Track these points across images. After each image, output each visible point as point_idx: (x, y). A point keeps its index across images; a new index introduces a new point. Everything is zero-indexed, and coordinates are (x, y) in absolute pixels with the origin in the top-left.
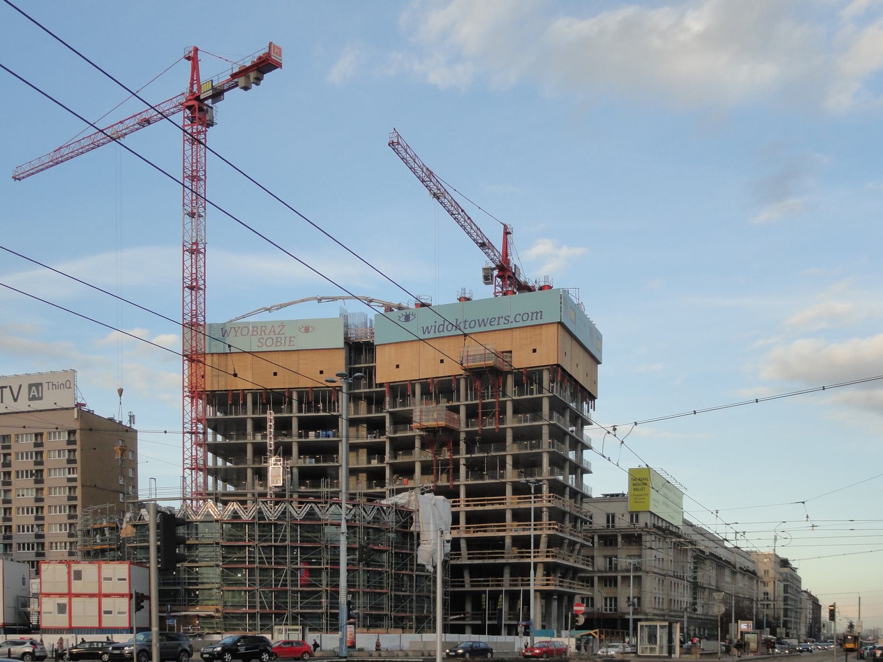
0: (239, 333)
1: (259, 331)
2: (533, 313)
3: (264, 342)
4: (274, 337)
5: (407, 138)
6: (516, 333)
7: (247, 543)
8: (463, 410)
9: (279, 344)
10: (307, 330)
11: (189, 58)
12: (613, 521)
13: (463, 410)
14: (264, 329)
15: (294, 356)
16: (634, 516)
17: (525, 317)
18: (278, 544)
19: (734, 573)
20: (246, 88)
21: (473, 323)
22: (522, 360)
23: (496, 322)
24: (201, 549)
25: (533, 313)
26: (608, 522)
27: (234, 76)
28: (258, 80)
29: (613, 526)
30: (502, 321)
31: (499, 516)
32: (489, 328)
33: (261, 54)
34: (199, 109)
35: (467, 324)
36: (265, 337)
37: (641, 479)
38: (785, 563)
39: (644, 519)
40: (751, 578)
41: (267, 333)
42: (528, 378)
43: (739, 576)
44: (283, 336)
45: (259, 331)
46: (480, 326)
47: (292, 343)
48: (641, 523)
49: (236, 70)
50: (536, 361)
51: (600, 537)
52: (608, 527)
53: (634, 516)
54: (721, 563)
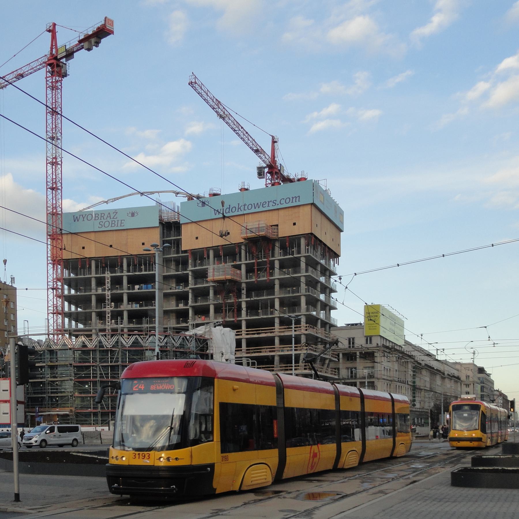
0: (85, 219)
2: (293, 198)
3: (103, 224)
6: (281, 212)
7: (91, 364)
8: (243, 267)
9: (113, 225)
10: (133, 215)
11: (49, 31)
12: (353, 343)
14: (103, 215)
16: (369, 339)
17: (288, 201)
18: (113, 364)
19: (443, 378)
20: (89, 49)
22: (286, 230)
25: (293, 198)
26: (350, 343)
27: (80, 42)
28: (97, 44)
29: (353, 347)
30: (271, 204)
31: (270, 341)
32: (261, 209)
33: (99, 25)
34: (56, 65)
35: (246, 207)
36: (104, 221)
37: (373, 313)
38: (481, 370)
39: (376, 341)
40: (456, 382)
43: (447, 380)
44: (116, 220)
45: (100, 217)
46: (255, 208)
48: (374, 344)
49: (82, 37)
51: (343, 354)
52: (350, 347)
53: (369, 339)
54: (433, 372)
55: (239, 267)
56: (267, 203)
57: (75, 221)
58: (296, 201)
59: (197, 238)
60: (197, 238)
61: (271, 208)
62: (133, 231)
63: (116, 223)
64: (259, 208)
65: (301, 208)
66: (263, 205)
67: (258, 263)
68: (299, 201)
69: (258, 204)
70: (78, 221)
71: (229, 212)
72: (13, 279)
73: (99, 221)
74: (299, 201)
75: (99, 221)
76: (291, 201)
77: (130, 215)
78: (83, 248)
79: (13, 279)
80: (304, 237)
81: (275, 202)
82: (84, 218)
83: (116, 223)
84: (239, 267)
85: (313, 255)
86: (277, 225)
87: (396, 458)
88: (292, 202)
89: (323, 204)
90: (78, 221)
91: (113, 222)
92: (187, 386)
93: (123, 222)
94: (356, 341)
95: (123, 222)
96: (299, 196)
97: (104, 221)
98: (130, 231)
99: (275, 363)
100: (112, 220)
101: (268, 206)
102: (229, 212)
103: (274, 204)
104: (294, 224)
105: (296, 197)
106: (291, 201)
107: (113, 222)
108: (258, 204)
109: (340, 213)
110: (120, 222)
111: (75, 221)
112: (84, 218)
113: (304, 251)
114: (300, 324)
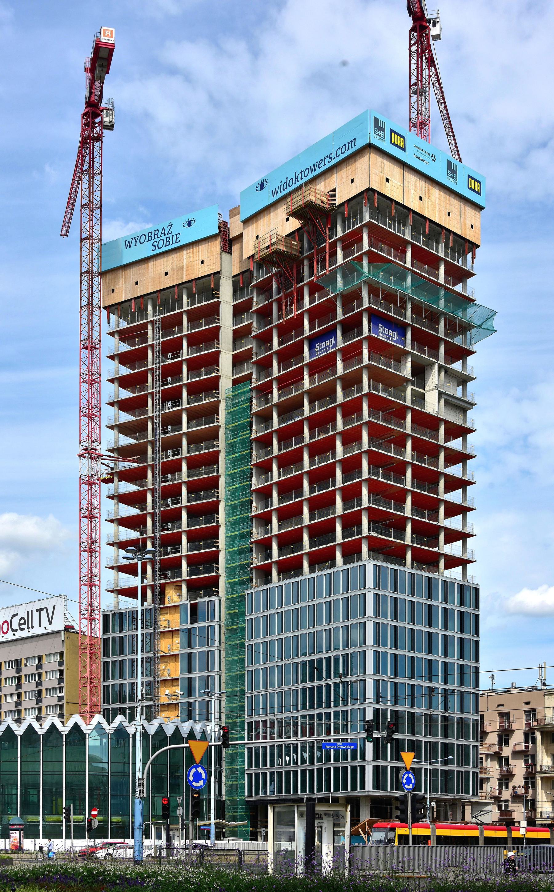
4: (163, 237)
9: (168, 243)
23: (323, 164)
32: (318, 171)
36: (157, 240)
44: (170, 235)
56: (324, 160)
57: (126, 248)
63: (171, 241)
64: (315, 170)
65: (151, 264)
66: (319, 165)
70: (130, 247)
72: (287, 220)
73: (153, 241)
75: (153, 241)
77: (186, 225)
78: (137, 283)
79: (287, 220)
82: (136, 242)
83: (171, 241)
87: (481, 327)
90: (130, 247)
92: (276, 820)
95: (178, 236)
97: (157, 240)
99: (407, 833)
100: (167, 236)
107: (168, 239)
110: (175, 237)
111: (126, 248)
112: (136, 242)
114: (408, 836)
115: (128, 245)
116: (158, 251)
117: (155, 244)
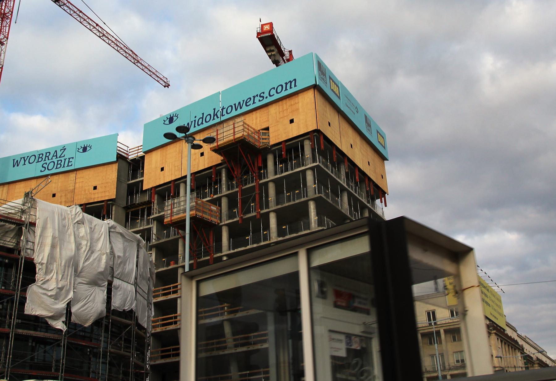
0: (27, 162)
1: (44, 157)
2: (286, 84)
3: (46, 166)
4: (55, 160)
5: (280, 33)
6: (273, 109)
8: (224, 202)
9: (59, 166)
10: (85, 149)
12: (434, 318)
13: (224, 202)
14: (48, 154)
15: (72, 175)
17: (279, 89)
21: (230, 108)
22: (280, 133)
23: (252, 102)
24: (357, 300)
25: (286, 84)
26: (429, 319)
29: (435, 324)
30: (257, 99)
32: (245, 109)
35: (225, 110)
36: (48, 162)
41: (50, 158)
42: (291, 150)
44: (63, 159)
45: (44, 157)
46: (236, 110)
47: (70, 164)
50: (294, 131)
51: (446, 331)
52: (430, 324)
55: (217, 202)
57: (14, 166)
58: (291, 88)
59: (162, 169)
60: (162, 169)
61: (258, 104)
62: (84, 171)
64: (241, 108)
66: (246, 103)
67: (243, 192)
68: (295, 86)
69: (239, 103)
70: (18, 166)
71: (202, 123)
74: (295, 86)
76: (284, 89)
77: (81, 150)
80: (308, 139)
81: (262, 95)
82: (25, 161)
84: (217, 202)
85: (332, 172)
86: (267, 129)
88: (286, 89)
89: (339, 98)
90: (18, 166)
91: (59, 162)
93: (71, 160)
94: (438, 316)
95: (71, 160)
96: (295, 80)
97: (48, 162)
98: (80, 172)
100: (59, 159)
101: (254, 103)
102: (202, 123)
103: (261, 99)
104: (292, 121)
105: (291, 82)
106: (284, 89)
107: (59, 162)
108: (239, 103)
109: (385, 134)
111: (14, 166)
112: (25, 161)
113: (309, 162)
115: (16, 163)
116: (47, 172)
117: (45, 165)
